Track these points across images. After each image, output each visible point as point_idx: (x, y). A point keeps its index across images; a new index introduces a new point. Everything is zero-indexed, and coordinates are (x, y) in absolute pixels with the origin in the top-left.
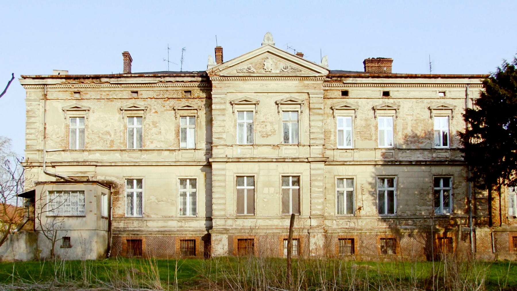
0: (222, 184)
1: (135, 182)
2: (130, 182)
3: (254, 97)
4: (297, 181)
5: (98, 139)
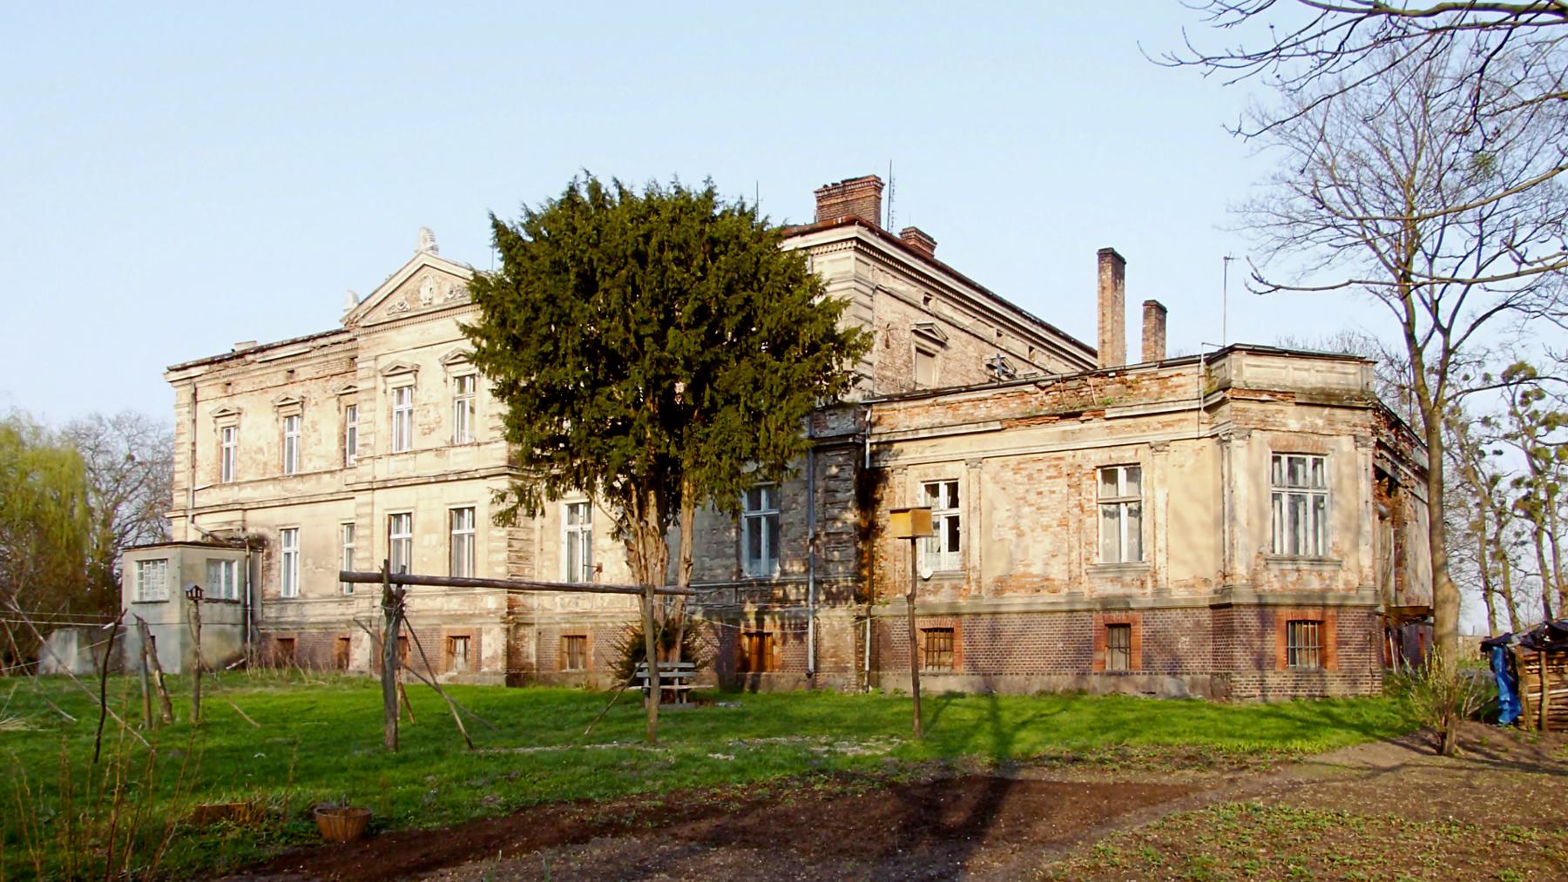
1: (1122, 473)
3: (407, 360)
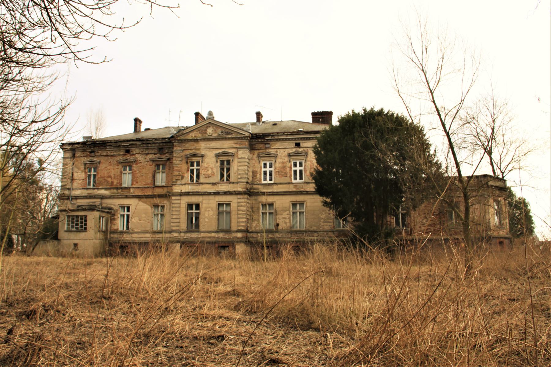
0: (178, 209)
2: (123, 207)
4: (198, 206)
5: (104, 181)
